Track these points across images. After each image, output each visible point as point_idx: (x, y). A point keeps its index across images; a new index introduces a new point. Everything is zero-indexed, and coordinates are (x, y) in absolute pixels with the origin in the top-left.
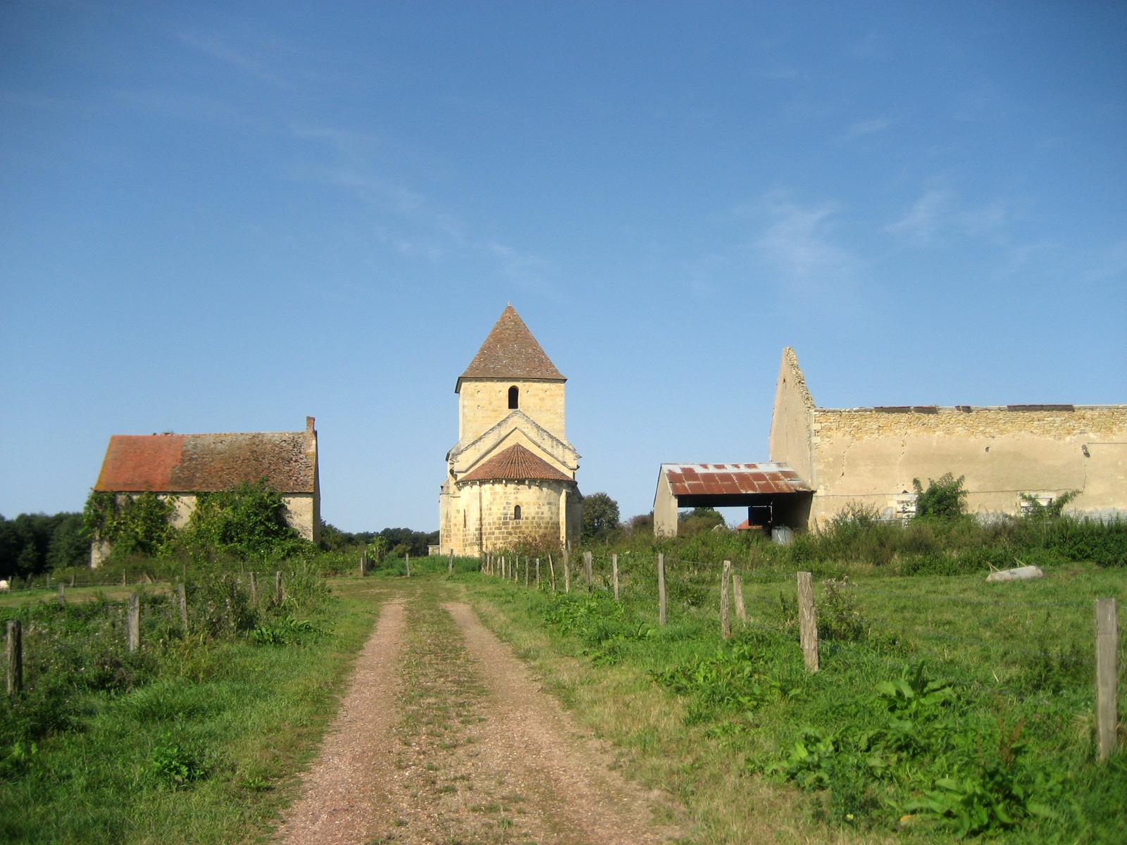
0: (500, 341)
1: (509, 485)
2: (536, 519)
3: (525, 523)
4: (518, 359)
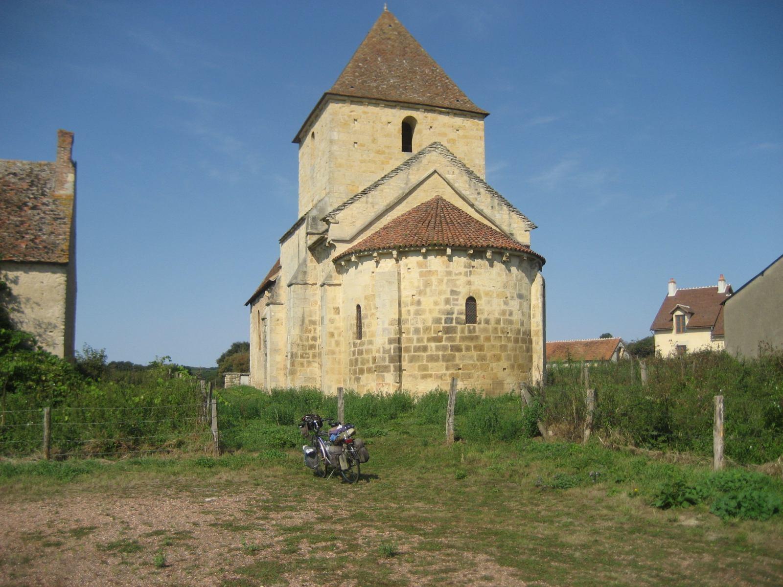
0: (380, 53)
1: (455, 258)
2: (502, 325)
3: (485, 330)
4: (411, 80)
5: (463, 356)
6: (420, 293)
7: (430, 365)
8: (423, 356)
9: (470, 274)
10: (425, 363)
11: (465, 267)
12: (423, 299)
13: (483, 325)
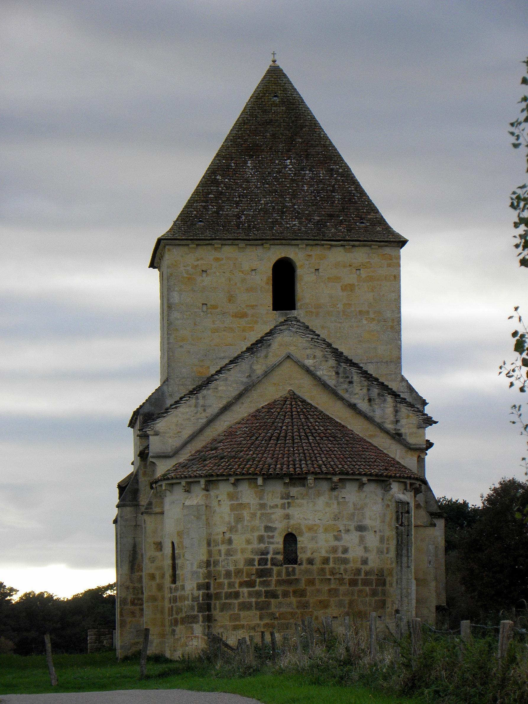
2: (331, 565)
3: (308, 572)
5: (280, 603)
6: (232, 529)
7: (243, 614)
8: (234, 604)
9: (289, 507)
10: (236, 612)
11: (282, 498)
12: (234, 537)
13: (304, 566)
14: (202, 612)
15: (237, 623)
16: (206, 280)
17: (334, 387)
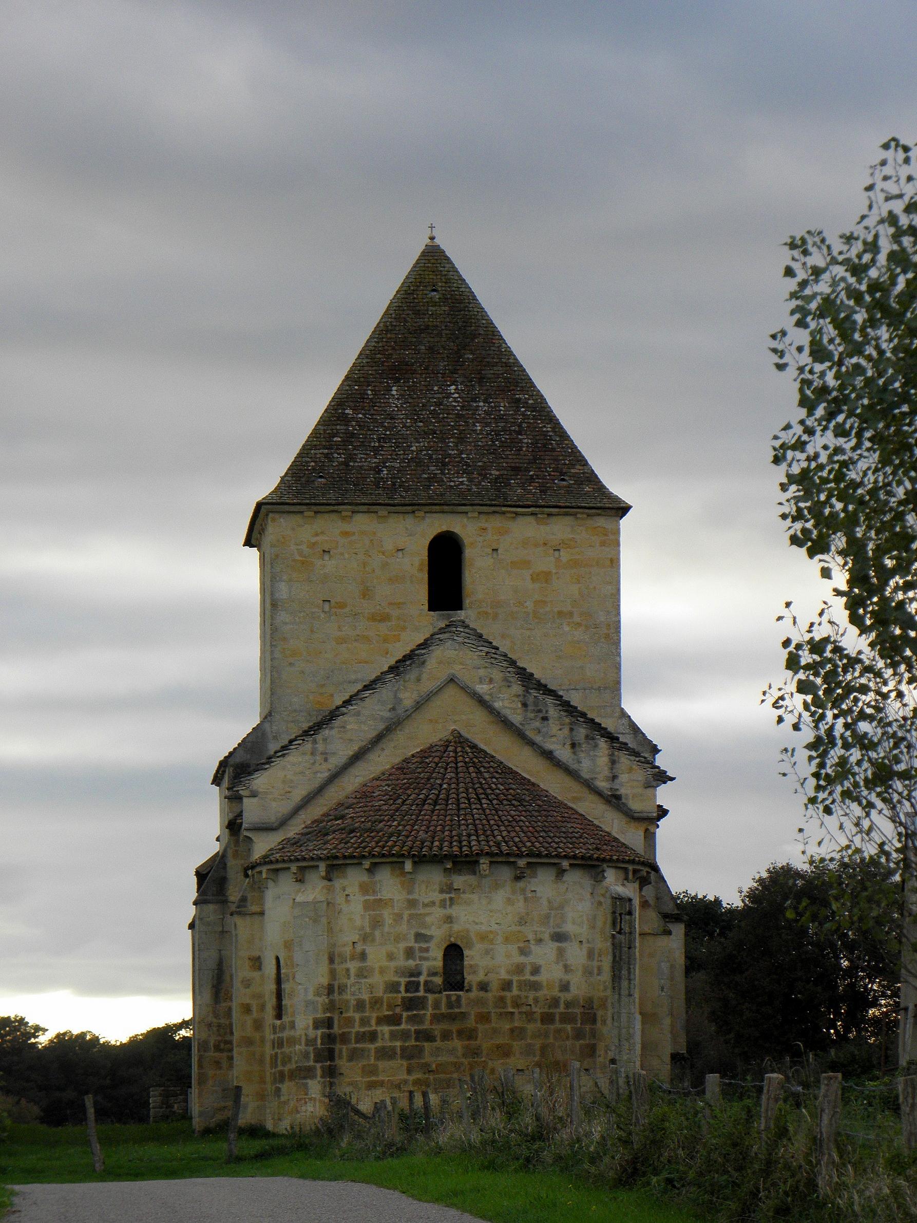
2: (515, 991)
3: (480, 1002)
5: (438, 1048)
7: (382, 1065)
8: (369, 1050)
9: (451, 905)
10: (372, 1061)
11: (442, 891)
12: (369, 950)
13: (474, 994)
14: (322, 1062)
15: (374, 1078)
16: (330, 565)
17: (520, 727)
